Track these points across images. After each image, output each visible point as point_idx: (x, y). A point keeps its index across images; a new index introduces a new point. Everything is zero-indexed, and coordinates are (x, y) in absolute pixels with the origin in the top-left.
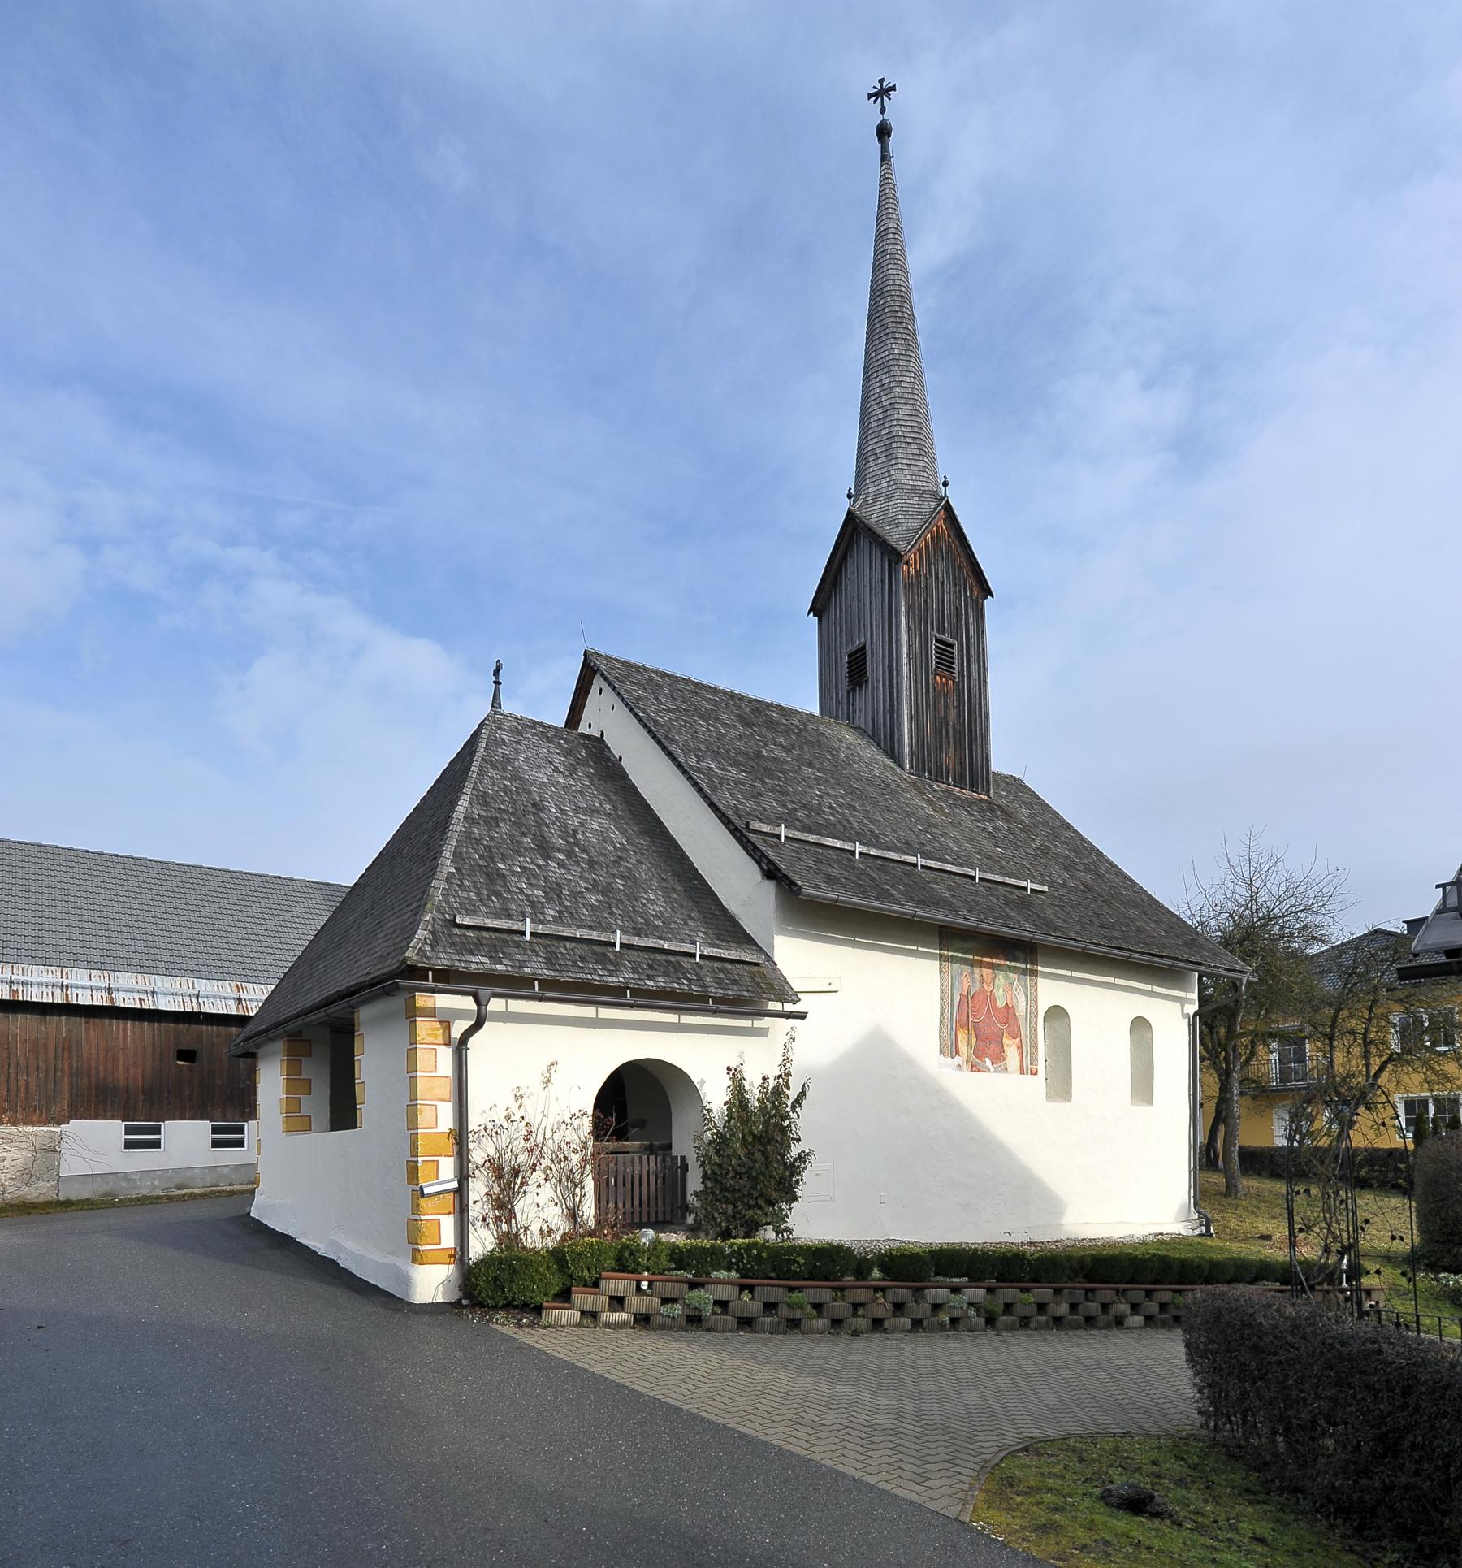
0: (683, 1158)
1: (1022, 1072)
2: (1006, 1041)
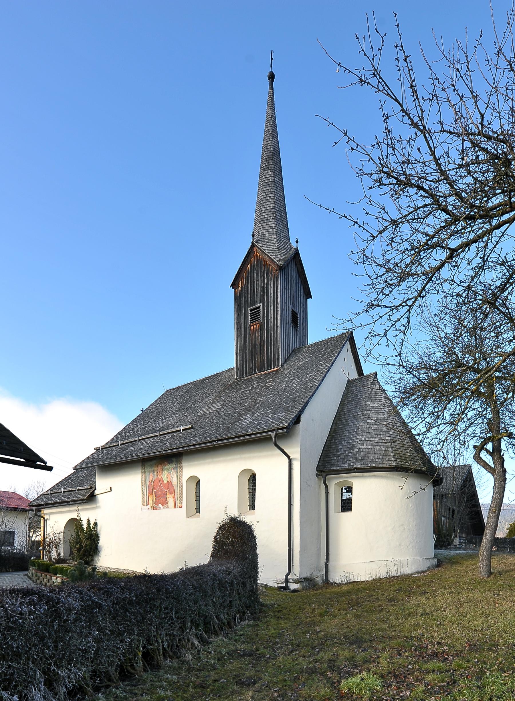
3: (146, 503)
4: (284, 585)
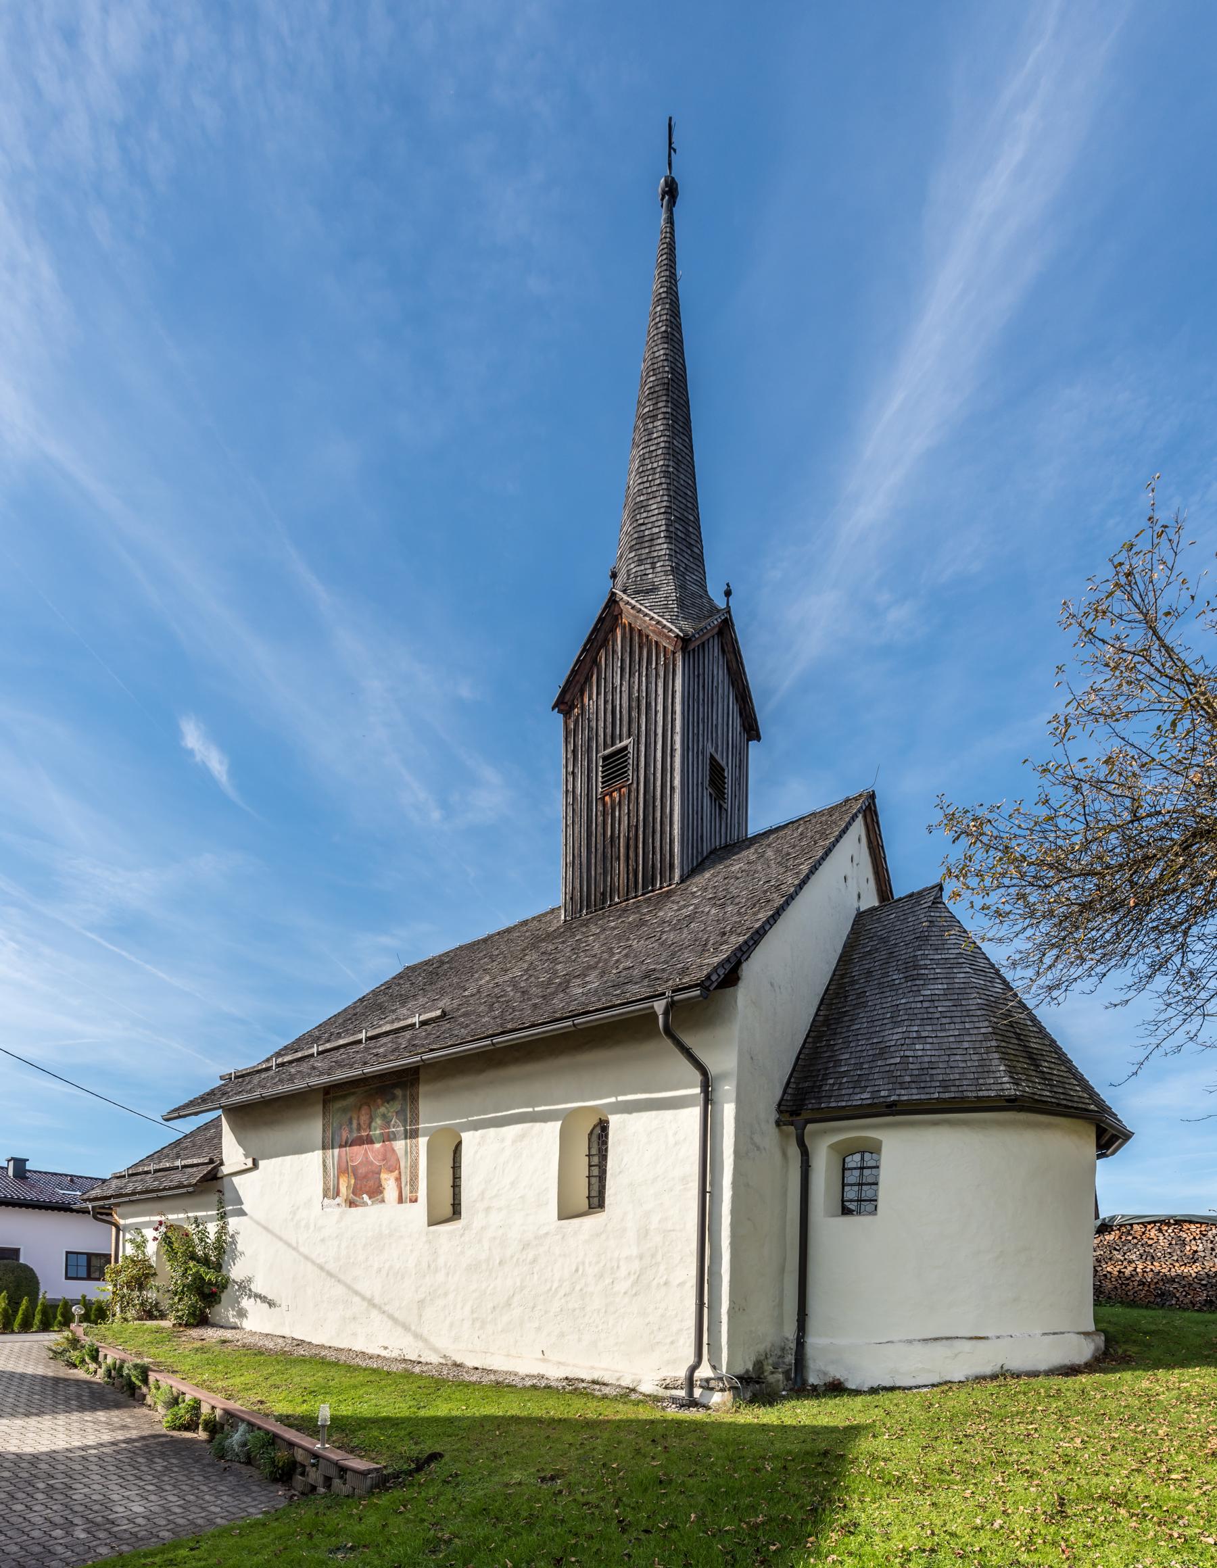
3: (331, 1192)
4: (682, 1393)
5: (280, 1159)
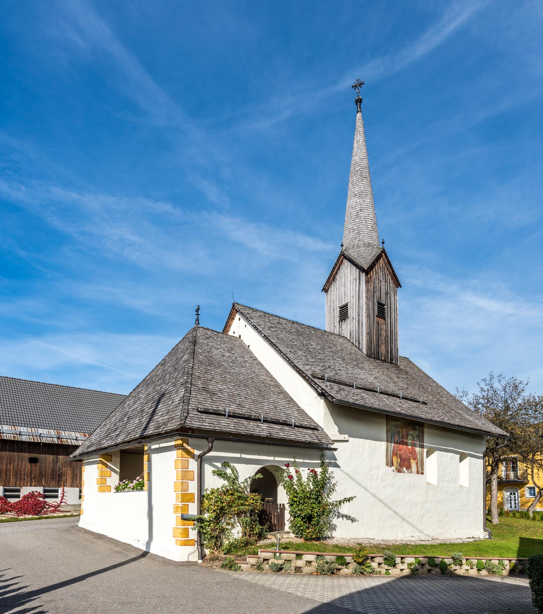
0: (283, 505)
1: (418, 473)
2: (412, 461)
5: (363, 440)
